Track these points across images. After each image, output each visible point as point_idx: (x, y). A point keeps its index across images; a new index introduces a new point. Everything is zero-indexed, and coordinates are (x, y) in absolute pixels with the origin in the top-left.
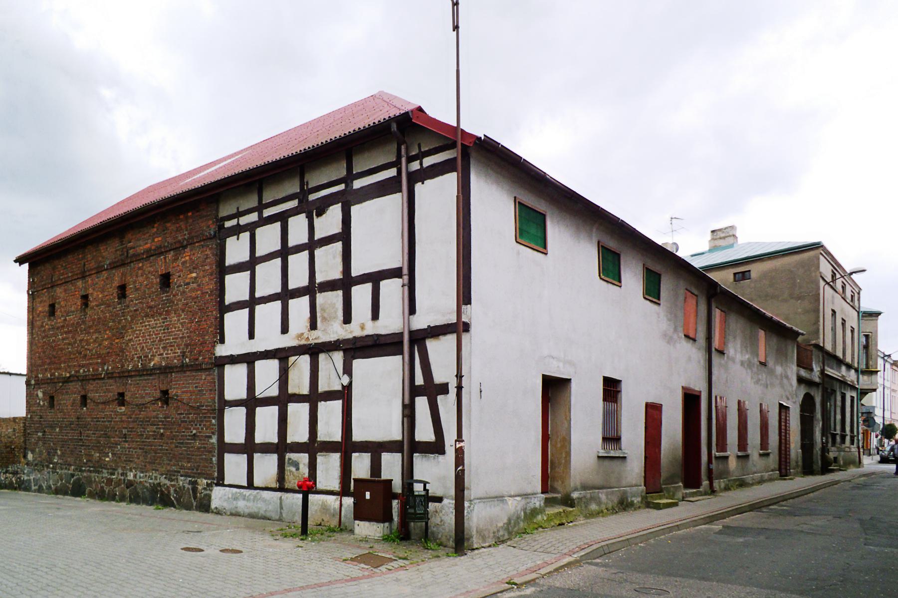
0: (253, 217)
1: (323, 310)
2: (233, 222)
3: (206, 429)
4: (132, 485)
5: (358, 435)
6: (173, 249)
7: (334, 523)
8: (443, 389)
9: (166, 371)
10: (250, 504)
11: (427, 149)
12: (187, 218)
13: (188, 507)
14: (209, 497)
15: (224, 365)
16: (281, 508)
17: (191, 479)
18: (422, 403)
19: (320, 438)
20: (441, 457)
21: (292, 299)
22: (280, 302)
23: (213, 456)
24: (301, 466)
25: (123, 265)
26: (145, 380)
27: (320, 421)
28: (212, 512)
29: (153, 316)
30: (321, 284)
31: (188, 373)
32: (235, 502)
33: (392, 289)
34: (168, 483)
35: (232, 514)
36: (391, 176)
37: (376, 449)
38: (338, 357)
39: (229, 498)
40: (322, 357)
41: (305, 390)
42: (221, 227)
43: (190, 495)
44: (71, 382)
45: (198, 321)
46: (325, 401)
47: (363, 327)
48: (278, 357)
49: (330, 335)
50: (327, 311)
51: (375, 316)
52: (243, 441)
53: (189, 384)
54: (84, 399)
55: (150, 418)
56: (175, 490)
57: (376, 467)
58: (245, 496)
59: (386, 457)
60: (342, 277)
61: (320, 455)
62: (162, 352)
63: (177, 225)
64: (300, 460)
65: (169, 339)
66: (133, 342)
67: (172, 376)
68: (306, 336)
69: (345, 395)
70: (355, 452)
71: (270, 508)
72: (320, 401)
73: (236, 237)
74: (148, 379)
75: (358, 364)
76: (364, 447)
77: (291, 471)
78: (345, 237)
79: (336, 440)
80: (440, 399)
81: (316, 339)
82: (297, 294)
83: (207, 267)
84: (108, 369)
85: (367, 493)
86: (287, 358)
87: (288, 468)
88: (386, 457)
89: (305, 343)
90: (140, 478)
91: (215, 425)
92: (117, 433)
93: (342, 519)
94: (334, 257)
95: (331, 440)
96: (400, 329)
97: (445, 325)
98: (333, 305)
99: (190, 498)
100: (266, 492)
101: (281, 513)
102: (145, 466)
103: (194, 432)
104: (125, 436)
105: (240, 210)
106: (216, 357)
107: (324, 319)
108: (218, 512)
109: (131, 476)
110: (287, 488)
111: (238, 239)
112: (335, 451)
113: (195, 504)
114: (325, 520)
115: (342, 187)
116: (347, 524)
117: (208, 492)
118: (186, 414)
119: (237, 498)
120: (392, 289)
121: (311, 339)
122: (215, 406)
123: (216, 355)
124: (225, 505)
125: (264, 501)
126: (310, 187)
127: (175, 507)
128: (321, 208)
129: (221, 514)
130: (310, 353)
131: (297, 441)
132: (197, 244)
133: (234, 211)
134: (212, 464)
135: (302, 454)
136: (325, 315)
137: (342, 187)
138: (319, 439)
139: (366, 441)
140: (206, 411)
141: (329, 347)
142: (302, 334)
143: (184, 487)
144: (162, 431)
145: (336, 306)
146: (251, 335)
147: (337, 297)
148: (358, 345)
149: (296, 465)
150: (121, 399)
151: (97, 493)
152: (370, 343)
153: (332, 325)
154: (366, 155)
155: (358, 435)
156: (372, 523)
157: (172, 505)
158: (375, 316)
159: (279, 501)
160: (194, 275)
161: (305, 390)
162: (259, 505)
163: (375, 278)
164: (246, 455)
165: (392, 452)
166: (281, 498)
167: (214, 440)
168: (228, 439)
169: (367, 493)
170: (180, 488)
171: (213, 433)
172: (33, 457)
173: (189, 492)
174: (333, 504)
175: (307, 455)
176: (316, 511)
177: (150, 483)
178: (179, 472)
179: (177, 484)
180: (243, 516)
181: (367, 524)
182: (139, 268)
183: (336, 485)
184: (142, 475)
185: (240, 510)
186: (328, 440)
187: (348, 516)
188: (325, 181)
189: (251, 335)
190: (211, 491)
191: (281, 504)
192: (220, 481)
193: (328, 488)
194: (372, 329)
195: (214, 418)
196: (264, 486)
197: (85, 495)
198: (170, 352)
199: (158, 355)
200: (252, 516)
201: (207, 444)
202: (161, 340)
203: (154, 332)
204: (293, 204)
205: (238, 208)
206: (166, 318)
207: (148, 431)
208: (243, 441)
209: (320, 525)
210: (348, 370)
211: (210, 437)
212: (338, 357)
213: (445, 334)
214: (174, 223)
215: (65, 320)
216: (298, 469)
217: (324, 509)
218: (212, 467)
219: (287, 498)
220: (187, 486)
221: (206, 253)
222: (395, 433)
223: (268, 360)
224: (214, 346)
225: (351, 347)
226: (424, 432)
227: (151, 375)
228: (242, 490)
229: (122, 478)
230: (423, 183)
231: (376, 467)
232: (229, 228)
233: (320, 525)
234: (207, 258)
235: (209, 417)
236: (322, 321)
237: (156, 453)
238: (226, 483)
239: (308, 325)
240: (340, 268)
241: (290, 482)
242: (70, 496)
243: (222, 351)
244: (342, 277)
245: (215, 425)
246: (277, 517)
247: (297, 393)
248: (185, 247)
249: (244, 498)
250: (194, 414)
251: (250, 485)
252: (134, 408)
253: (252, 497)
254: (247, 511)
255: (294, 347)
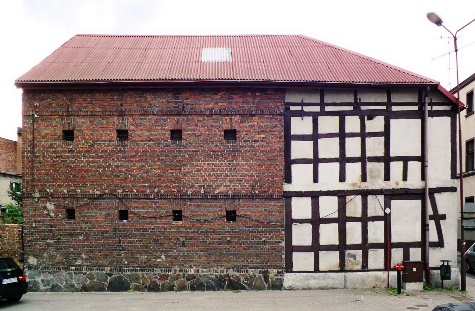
0: (317, 109)
1: (371, 172)
2: (299, 108)
3: (276, 237)
4: (195, 278)
5: (395, 239)
6: (239, 115)
7: (385, 285)
8: (431, 218)
9: (235, 197)
10: (321, 281)
11: (435, 102)
12: (255, 97)
13: (260, 288)
14: (281, 280)
15: (318, 197)
16: (345, 281)
17: (261, 270)
18: (432, 224)
19: (370, 241)
20: (442, 249)
21: (349, 162)
22: (360, 163)
23: (283, 254)
24: (357, 257)
25: (179, 115)
26: (208, 202)
27: (370, 232)
28: (285, 289)
29: (217, 158)
30: (369, 157)
31: (257, 200)
32: (307, 282)
33: (414, 167)
34: (238, 274)
35: (304, 289)
36: (415, 109)
37: (406, 247)
38: (381, 198)
39: (301, 279)
40: (370, 198)
41: (359, 215)
42: (287, 109)
43: (262, 280)
44: (103, 199)
45: (267, 167)
46: (373, 221)
47: (397, 184)
48: (338, 195)
49: (375, 185)
50: (374, 173)
51: (405, 178)
52: (311, 244)
53: (258, 207)
54: (123, 215)
55: (215, 230)
56: (246, 279)
57: (406, 255)
58: (316, 277)
59: (412, 250)
60: (384, 156)
61: (371, 251)
62: (228, 184)
63: (427, 104)
64: (357, 254)
65: (238, 176)
66: (193, 174)
67: (239, 201)
68: (358, 184)
69: (386, 219)
70: (393, 248)
71: (337, 282)
72: (369, 221)
73: (300, 118)
74: (213, 202)
75: (394, 203)
76: (398, 245)
77: (349, 260)
78: (386, 134)
79: (381, 242)
80: (442, 222)
81: (365, 187)
82: (352, 161)
83: (276, 133)
84: (159, 192)
85: (414, 268)
86: (345, 197)
87: (348, 259)
88: (412, 250)
89: (358, 189)
90: (203, 272)
91: (284, 235)
92: (173, 240)
93: (389, 283)
94: (380, 144)
95: (377, 242)
96: (422, 187)
97: (445, 188)
98: (378, 170)
99: (262, 282)
100: (330, 273)
101: (345, 284)
102: (209, 263)
103: (264, 239)
104: (183, 243)
105: (304, 102)
106: (285, 192)
107: (372, 177)
108: (291, 289)
109: (192, 272)
110: (346, 270)
111: (302, 120)
112: (381, 248)
113: (267, 286)
114: (378, 284)
115: (385, 107)
116: (392, 285)
117: (279, 277)
118: (254, 227)
119: (308, 279)
120: (414, 167)
121: (362, 187)
122: (283, 222)
123: (284, 190)
124: (298, 284)
125: (333, 278)
126: (362, 101)
127: (246, 289)
128: (372, 115)
129: (294, 290)
130: (363, 194)
131: (354, 243)
132: (265, 116)
133: (299, 101)
134: (282, 259)
135: (357, 251)
136: (373, 175)
137: (385, 107)
138: (369, 242)
139: (400, 243)
140: (276, 226)
141: (375, 192)
142: (356, 184)
143: (255, 276)
144: (228, 239)
145: (381, 171)
146: (316, 180)
147: (381, 166)
148: (396, 193)
149: (354, 257)
150: (178, 215)
151: (146, 287)
152: (403, 192)
153: (377, 181)
154: (399, 95)
155: (395, 239)
156: (416, 283)
157: (244, 288)
158: (405, 178)
159: (343, 277)
160: (262, 136)
161: (359, 215)
162: (328, 281)
163: (405, 160)
164: (313, 253)
165: (415, 247)
166: (345, 276)
167: (283, 244)
168: (295, 242)
169: (414, 268)
170: (251, 277)
171: (283, 240)
172: (37, 262)
173: (261, 279)
174: (382, 276)
175: (361, 251)
176: (372, 281)
177: (216, 276)
178: (248, 266)
179: (198, 274)
180: (314, 289)
181: (413, 284)
182: (200, 121)
183: (381, 265)
184: (205, 270)
185: (310, 286)
186: (376, 242)
187: (393, 281)
188: (373, 101)
189: (316, 180)
190: (283, 276)
191: (345, 279)
192: (289, 268)
193: (376, 268)
194: (402, 185)
195: (283, 230)
196: (328, 270)
197: (130, 289)
198: (237, 185)
199: (224, 186)
200: (321, 288)
201: (276, 246)
202: (226, 176)
203: (218, 169)
204: (351, 108)
205: (302, 100)
206: (233, 161)
207: (211, 239)
208: (311, 244)
209: (375, 287)
210: (387, 205)
211: (280, 242)
212: (381, 198)
213: (445, 192)
214: (241, 97)
215: (92, 146)
216: (355, 259)
217: (377, 279)
218: (281, 261)
219: (350, 275)
220: (257, 275)
221: (275, 123)
222: (418, 238)
223: (330, 197)
224: (282, 185)
225: (391, 193)
226: (433, 236)
227: (216, 199)
228: (311, 274)
229: (182, 273)
230: (432, 118)
231: (406, 255)
232: (293, 111)
233: (375, 287)
234: (275, 127)
235: (279, 230)
236: (370, 178)
237: (221, 254)
238: (294, 270)
239: (361, 179)
240: (383, 151)
241: (349, 266)
242: (107, 291)
243: (287, 188)
244: (384, 156)
245: (284, 235)
246: (343, 287)
247: (353, 216)
248: (254, 115)
249: (315, 278)
250: (263, 227)
251: (317, 269)
252: (194, 222)
253: (322, 277)
254: (317, 286)
255: (351, 191)
